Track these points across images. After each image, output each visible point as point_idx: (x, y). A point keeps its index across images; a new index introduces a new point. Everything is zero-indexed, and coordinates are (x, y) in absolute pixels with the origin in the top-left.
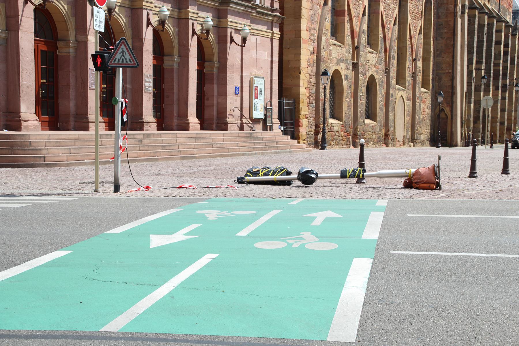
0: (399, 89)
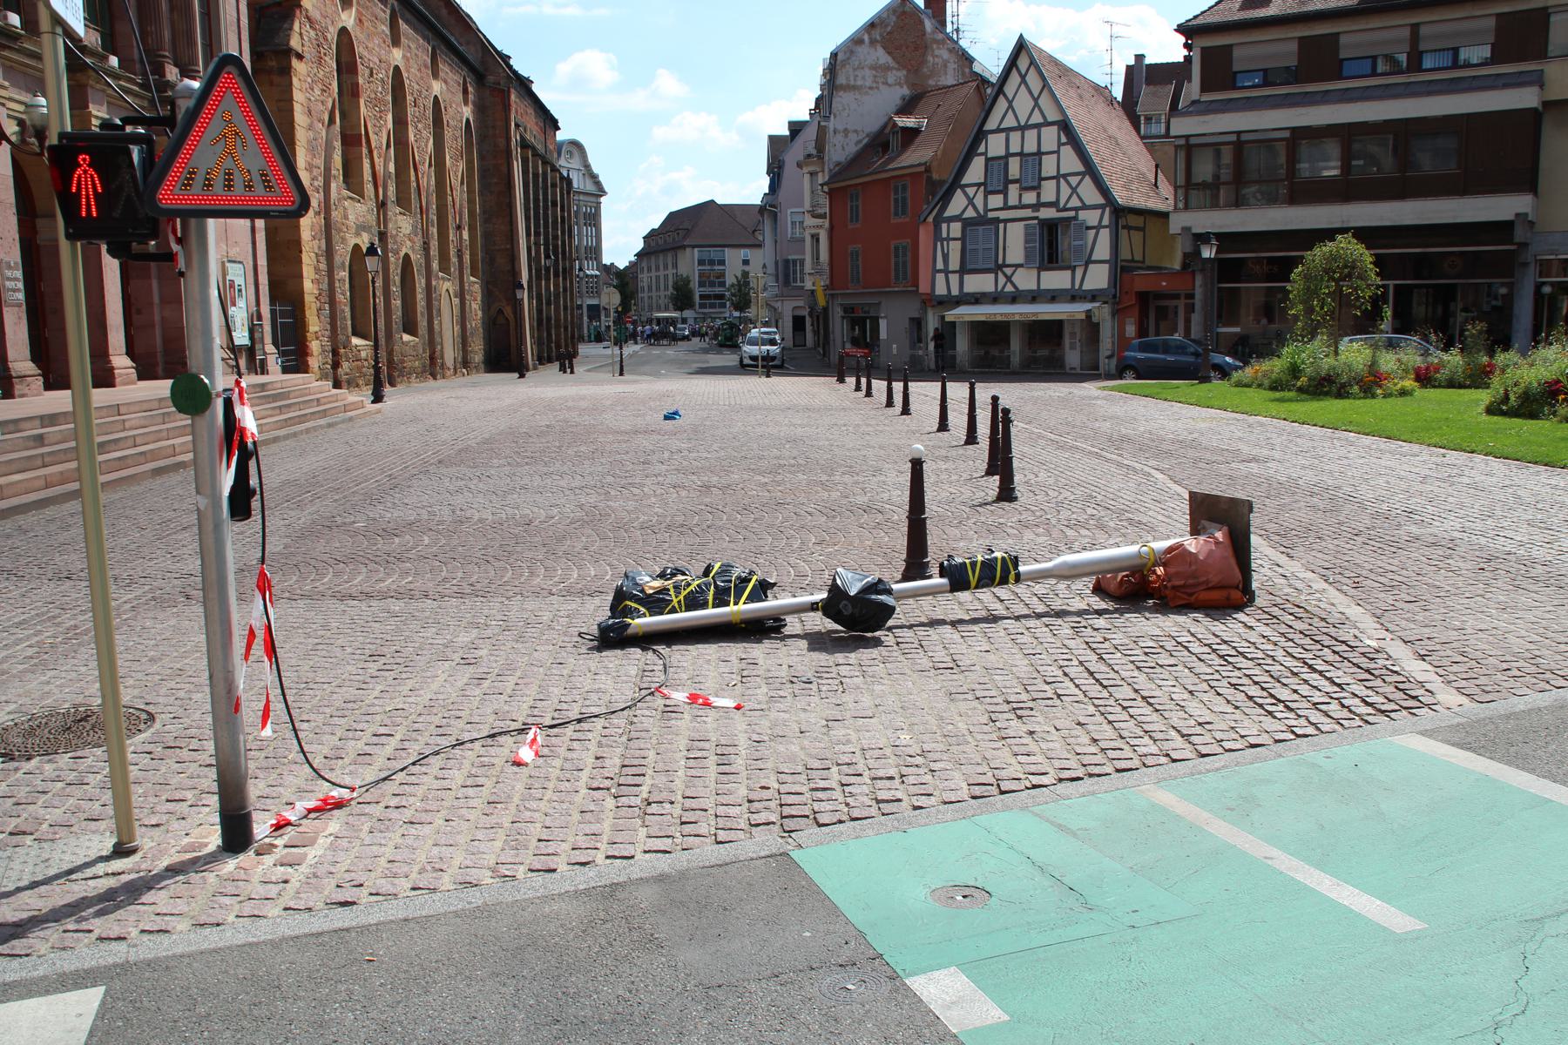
0: (443, 278)
